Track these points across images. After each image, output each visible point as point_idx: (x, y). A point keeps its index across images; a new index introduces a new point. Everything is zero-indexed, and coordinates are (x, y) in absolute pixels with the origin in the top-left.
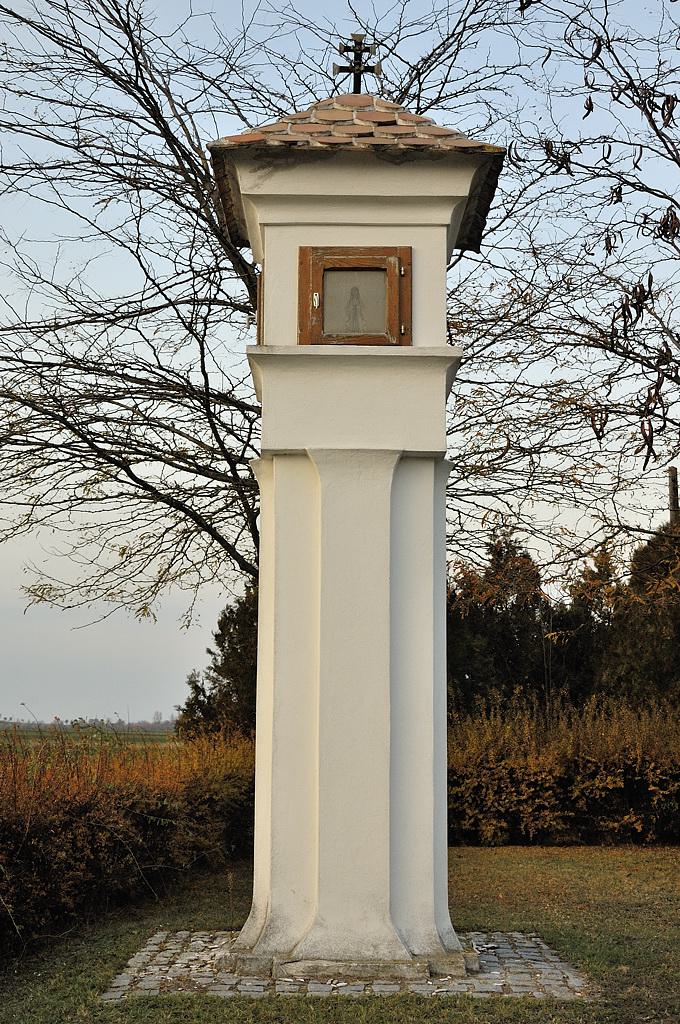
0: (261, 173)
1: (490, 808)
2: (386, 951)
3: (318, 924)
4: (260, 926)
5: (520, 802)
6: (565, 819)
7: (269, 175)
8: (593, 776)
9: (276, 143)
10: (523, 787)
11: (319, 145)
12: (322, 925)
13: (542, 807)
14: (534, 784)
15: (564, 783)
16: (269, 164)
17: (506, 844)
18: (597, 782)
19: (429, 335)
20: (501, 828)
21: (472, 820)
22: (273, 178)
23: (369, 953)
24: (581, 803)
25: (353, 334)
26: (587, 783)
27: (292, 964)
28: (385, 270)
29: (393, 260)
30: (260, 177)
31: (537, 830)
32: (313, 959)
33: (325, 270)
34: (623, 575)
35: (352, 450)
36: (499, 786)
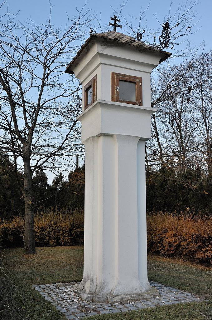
0: (103, 47)
1: (52, 237)
2: (139, 290)
3: (119, 283)
4: (95, 285)
5: (60, 235)
6: (70, 239)
7: (106, 48)
8: (77, 228)
9: (112, 38)
10: (61, 231)
11: (124, 41)
12: (120, 284)
13: (65, 236)
14: (64, 231)
15: (70, 230)
16: (106, 45)
17: (56, 246)
18: (78, 229)
19: (147, 104)
20: (55, 242)
21: (47, 240)
22: (107, 49)
23: (134, 291)
24: (74, 235)
25: (128, 101)
26: (76, 230)
27: (115, 298)
28: (136, 83)
29: (138, 80)
30: (103, 48)
31: (64, 242)
32: (120, 295)
33: (120, 80)
34: (66, 179)
35: (128, 136)
36: (55, 231)
